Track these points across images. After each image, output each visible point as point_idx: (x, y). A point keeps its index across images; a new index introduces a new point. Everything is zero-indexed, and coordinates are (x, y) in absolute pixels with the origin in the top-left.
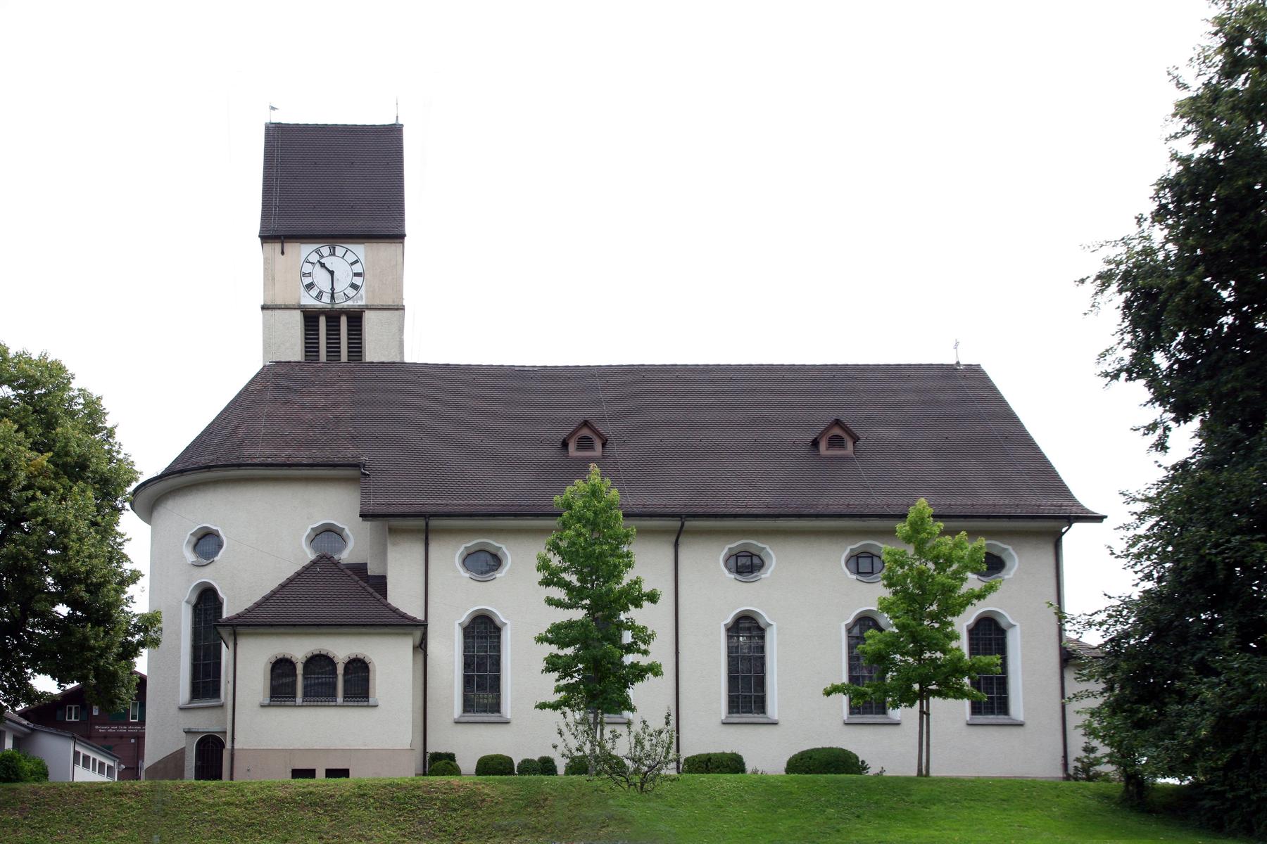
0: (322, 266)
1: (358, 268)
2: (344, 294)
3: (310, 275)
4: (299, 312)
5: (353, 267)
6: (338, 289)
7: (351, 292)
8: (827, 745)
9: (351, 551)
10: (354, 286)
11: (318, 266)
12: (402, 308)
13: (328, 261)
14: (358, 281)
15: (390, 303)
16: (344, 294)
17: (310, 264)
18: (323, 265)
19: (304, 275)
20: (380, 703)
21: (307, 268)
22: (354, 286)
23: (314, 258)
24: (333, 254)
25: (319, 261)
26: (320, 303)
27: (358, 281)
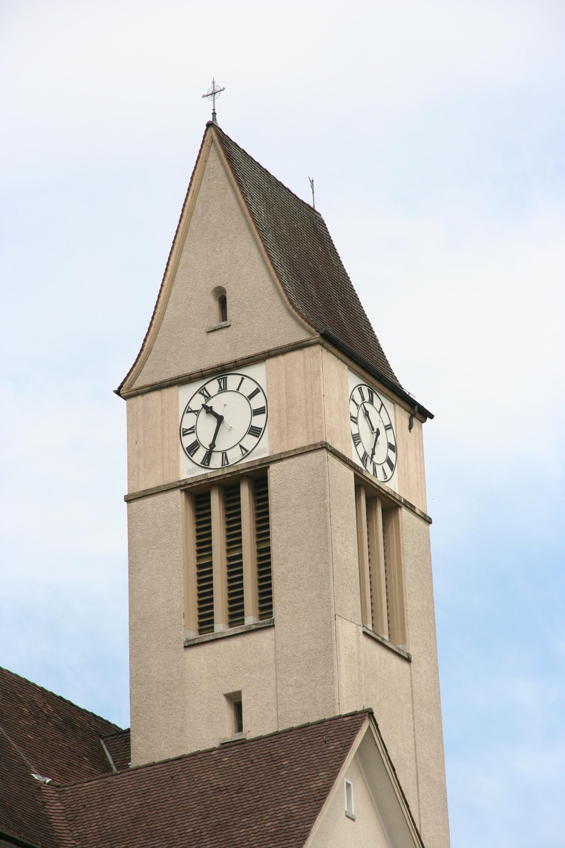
0: (207, 412)
1: (258, 402)
2: (241, 447)
3: (257, 412)
4: (178, 492)
5: (252, 401)
6: (220, 446)
7: (250, 442)
8: (101, 717)
9: (31, 846)
10: (255, 431)
11: (203, 413)
12: (128, 499)
13: (216, 404)
14: (259, 421)
15: (160, 483)
16: (241, 447)
17: (193, 409)
18: (209, 411)
19: (185, 432)
20: (356, 820)
21: (189, 421)
22: (255, 431)
23: (198, 402)
24: (223, 389)
25: (204, 406)
26: (208, 471)
27: (259, 421)
